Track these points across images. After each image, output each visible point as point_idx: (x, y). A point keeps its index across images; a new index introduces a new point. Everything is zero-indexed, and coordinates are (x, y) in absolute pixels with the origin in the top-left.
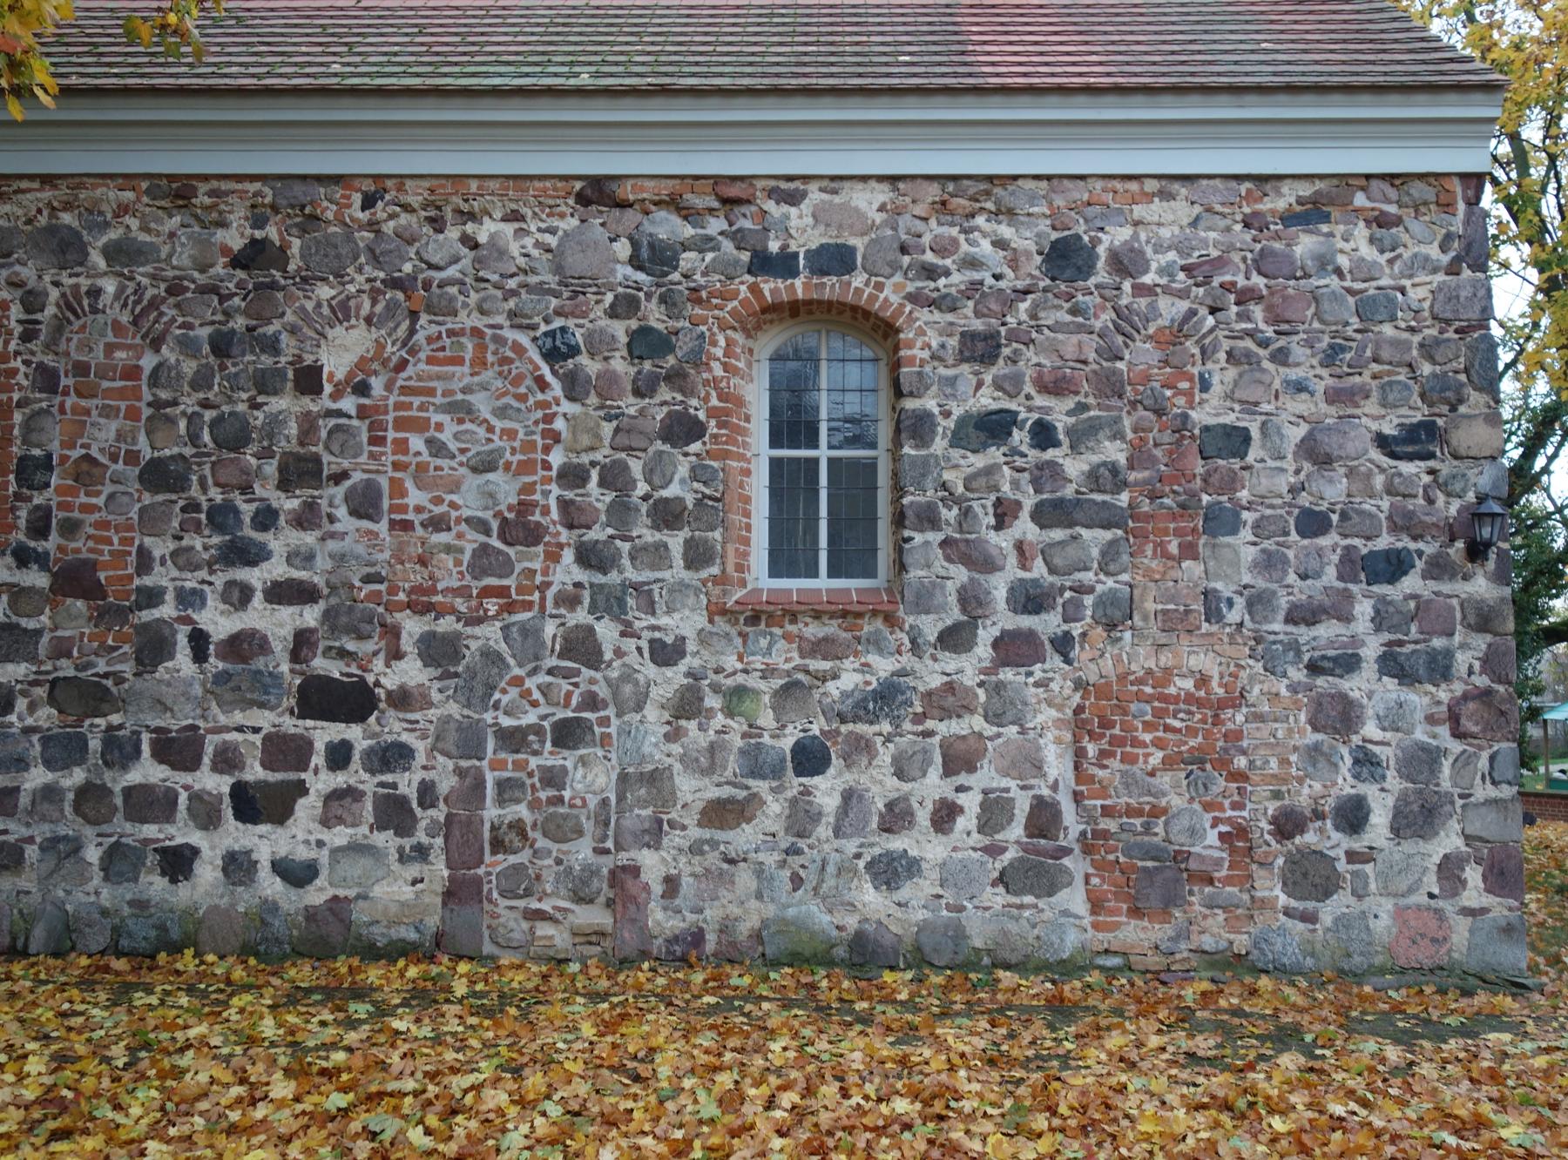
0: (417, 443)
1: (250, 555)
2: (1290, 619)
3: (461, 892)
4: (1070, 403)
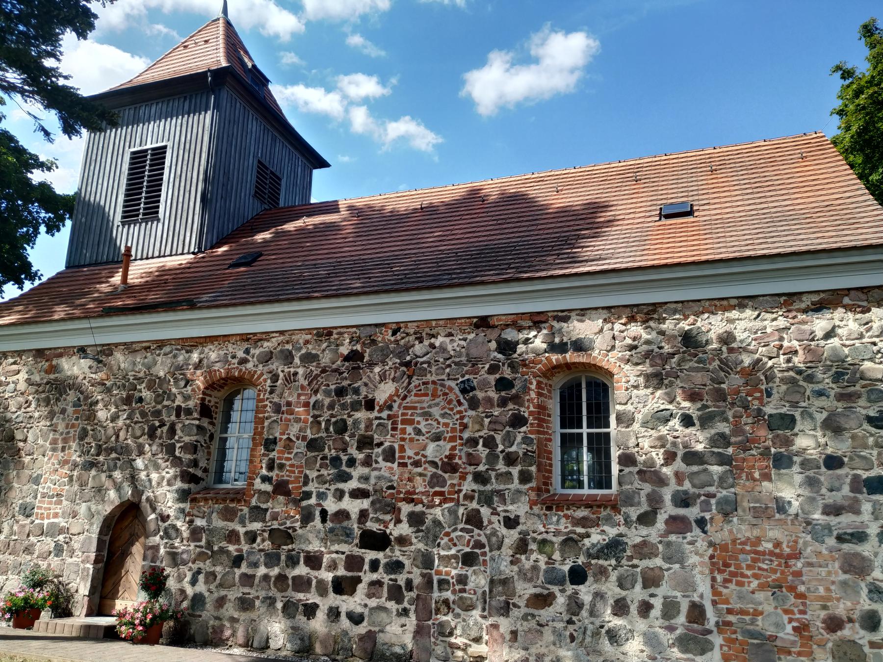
0: (409, 429)
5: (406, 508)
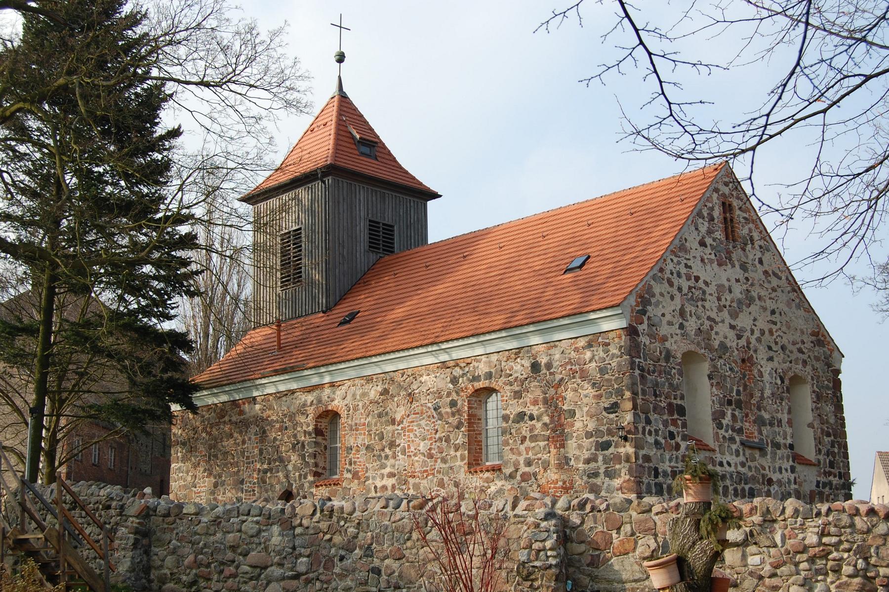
0: (412, 435)
1: (383, 466)
2: (584, 463)
3: (210, 212)
4: (537, 407)
5: (411, 481)
